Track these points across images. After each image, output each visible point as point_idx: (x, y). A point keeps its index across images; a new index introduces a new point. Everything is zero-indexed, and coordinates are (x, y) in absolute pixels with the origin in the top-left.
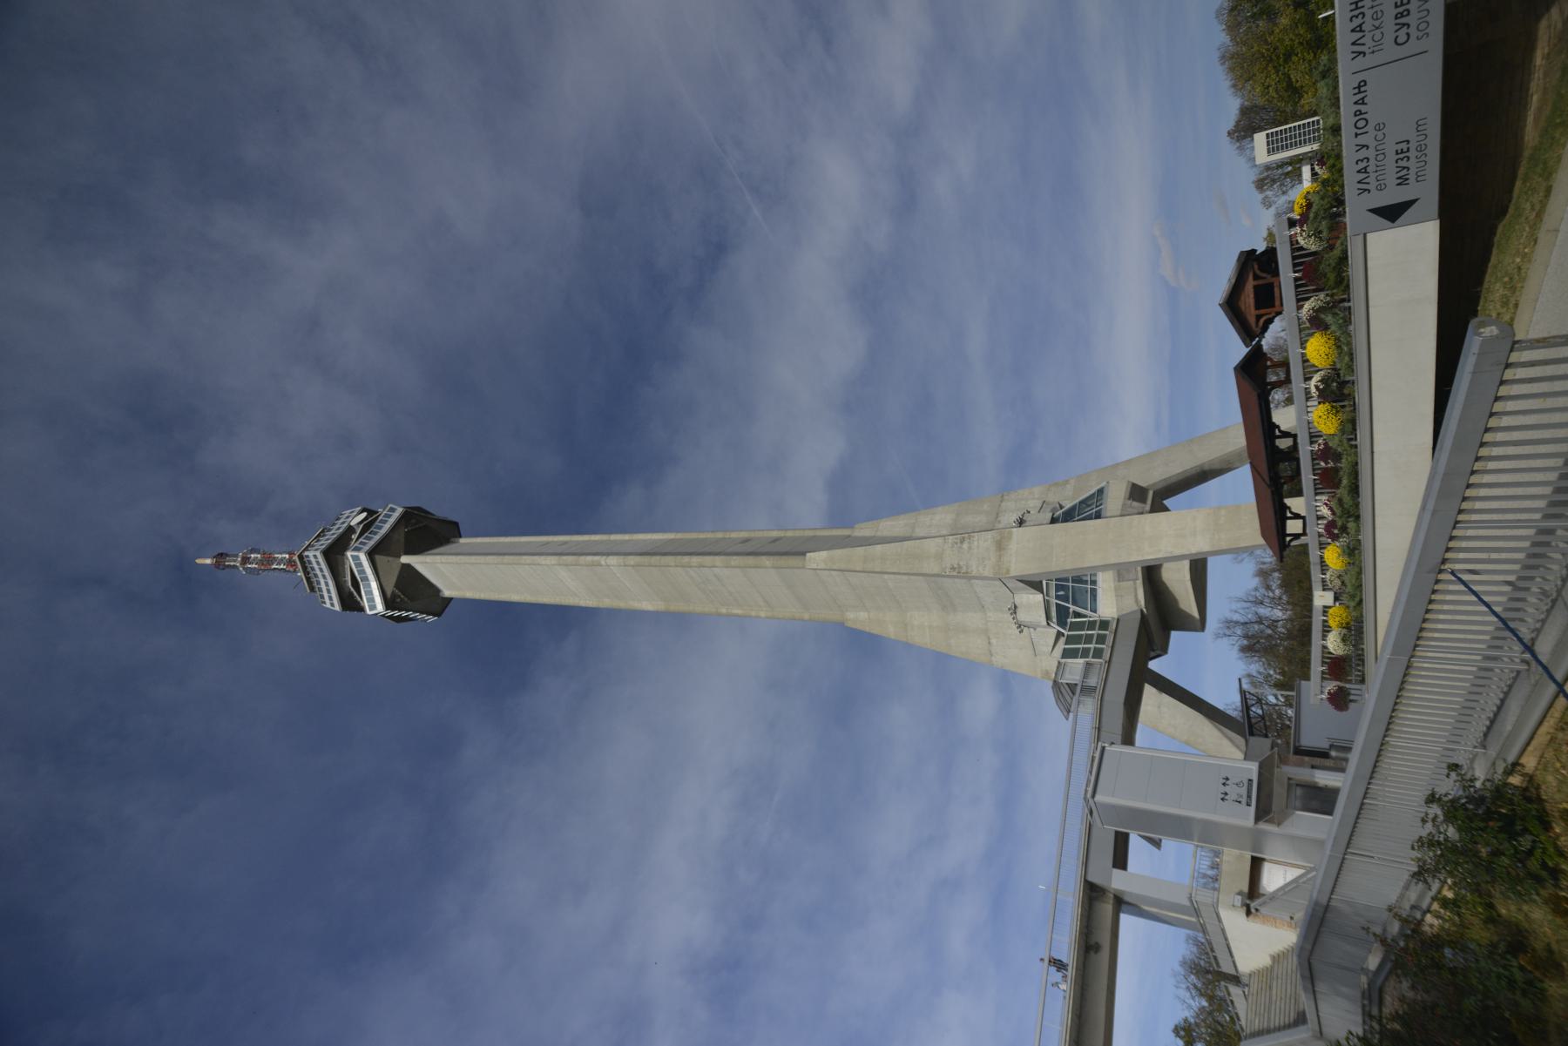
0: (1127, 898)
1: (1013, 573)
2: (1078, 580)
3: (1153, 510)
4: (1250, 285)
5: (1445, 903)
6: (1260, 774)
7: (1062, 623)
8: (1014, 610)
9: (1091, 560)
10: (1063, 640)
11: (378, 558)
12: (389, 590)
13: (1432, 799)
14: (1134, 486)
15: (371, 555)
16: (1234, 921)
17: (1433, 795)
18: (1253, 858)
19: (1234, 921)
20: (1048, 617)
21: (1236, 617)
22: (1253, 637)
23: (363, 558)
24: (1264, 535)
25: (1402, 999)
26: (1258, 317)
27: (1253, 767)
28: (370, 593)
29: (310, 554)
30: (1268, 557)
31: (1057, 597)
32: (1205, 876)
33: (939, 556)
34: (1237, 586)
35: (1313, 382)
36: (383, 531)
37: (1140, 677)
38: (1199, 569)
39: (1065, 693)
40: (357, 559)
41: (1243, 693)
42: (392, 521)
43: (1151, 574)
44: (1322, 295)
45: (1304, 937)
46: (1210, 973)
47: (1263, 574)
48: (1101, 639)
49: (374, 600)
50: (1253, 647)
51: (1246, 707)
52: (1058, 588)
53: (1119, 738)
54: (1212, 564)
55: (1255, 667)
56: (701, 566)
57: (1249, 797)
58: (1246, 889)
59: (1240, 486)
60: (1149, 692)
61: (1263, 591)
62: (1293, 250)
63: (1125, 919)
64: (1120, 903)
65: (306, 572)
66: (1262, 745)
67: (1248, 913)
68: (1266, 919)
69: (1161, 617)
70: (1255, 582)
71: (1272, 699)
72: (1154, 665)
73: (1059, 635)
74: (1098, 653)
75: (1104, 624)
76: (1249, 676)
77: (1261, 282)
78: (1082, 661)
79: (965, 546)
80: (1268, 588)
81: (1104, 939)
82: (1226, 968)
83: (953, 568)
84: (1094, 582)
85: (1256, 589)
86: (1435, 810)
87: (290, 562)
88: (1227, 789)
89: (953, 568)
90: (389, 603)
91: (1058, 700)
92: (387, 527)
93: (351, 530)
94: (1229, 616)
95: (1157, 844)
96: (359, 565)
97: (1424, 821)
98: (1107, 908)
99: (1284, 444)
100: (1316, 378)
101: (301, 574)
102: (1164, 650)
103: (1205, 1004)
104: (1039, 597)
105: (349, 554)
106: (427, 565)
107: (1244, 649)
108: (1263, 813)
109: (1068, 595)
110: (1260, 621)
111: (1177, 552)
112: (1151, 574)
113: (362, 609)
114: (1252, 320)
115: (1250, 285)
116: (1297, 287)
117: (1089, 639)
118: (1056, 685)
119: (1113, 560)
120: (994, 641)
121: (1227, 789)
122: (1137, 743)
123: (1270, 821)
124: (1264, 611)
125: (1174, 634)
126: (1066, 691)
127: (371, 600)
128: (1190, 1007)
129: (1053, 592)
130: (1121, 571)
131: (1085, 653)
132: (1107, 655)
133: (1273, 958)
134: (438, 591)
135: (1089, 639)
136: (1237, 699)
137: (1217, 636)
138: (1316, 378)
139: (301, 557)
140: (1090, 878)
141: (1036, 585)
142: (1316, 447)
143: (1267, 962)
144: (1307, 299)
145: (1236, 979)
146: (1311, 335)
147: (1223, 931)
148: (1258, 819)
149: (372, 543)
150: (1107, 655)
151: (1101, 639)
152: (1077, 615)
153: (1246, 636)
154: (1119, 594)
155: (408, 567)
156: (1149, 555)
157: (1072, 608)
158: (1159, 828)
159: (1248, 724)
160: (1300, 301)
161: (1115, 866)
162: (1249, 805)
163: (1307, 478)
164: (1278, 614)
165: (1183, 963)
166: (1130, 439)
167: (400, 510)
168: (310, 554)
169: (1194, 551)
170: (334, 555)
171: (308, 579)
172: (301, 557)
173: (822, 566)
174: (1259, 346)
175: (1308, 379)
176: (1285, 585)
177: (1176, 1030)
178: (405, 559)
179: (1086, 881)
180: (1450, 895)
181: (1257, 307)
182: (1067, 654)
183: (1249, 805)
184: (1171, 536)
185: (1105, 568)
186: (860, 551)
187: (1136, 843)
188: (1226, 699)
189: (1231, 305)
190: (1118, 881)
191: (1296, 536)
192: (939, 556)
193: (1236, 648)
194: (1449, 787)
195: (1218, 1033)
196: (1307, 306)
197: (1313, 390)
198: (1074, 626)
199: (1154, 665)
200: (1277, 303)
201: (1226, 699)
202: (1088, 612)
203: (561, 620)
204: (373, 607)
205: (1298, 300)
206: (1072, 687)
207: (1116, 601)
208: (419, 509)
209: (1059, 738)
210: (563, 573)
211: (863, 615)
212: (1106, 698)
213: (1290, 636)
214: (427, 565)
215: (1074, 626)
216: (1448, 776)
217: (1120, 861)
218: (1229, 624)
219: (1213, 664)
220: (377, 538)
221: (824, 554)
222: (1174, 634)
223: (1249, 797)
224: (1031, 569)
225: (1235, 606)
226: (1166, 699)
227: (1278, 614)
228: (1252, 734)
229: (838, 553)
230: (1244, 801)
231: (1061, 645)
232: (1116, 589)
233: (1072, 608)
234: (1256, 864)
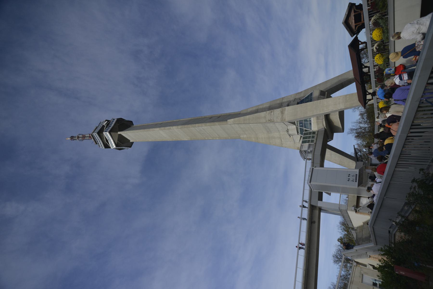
0: (322, 208)
1: (286, 120)
2: (306, 121)
3: (327, 97)
4: (353, 14)
5: (416, 211)
6: (359, 173)
7: (301, 134)
8: (288, 131)
9: (309, 114)
10: (302, 138)
11: (112, 133)
12: (116, 142)
13: (414, 181)
14: (321, 91)
15: (110, 132)
16: (352, 214)
17: (414, 179)
18: (357, 196)
19: (352, 214)
20: (298, 132)
21: (354, 128)
22: (358, 133)
23: (108, 133)
24: (359, 101)
25: (401, 237)
26: (356, 26)
27: (357, 171)
28: (111, 143)
29: (94, 134)
30: (362, 109)
31: (300, 126)
32: (346, 200)
33: (265, 117)
34: (354, 117)
35: (375, 47)
36: (112, 126)
37: (325, 147)
38: (341, 114)
39: (303, 153)
40: (107, 135)
41: (355, 149)
42: (114, 123)
43: (327, 117)
44: (378, 14)
45: (372, 219)
46: (346, 225)
47: (362, 115)
48: (313, 137)
49: (113, 145)
50: (359, 135)
51: (356, 153)
52: (300, 123)
53: (319, 165)
54: (346, 112)
55: (359, 142)
56: (199, 126)
57: (356, 179)
58: (355, 204)
59: (352, 88)
60: (328, 151)
61: (362, 119)
62: (372, 41)
63: (322, 214)
64: (320, 210)
65: (93, 138)
66: (361, 164)
67: (356, 212)
68: (361, 213)
69: (331, 129)
70: (360, 117)
71: (364, 150)
72: (329, 143)
73: (301, 136)
74: (312, 141)
75: (314, 133)
76: (358, 144)
77: (356, 13)
78: (308, 144)
79: (272, 113)
80: (363, 118)
81: (316, 220)
82: (350, 226)
83: (269, 120)
84: (310, 121)
85: (359, 119)
86: (415, 184)
87: (90, 137)
88: (349, 178)
89: (269, 120)
90: (117, 145)
91: (301, 155)
92: (113, 124)
93: (103, 126)
94: (352, 127)
95: (330, 194)
96: (107, 136)
97: (411, 189)
98: (317, 212)
99: (365, 70)
100: (376, 45)
101: (93, 140)
102: (332, 139)
103: (346, 233)
104: (295, 126)
105: (104, 133)
106: (126, 134)
107: (356, 137)
108: (360, 184)
109: (303, 126)
110: (361, 128)
111: (335, 109)
112: (327, 117)
113: (110, 148)
114: (354, 27)
115: (353, 14)
116: (369, 12)
117: (309, 137)
118: (301, 152)
119: (315, 114)
120: (283, 140)
121: (349, 178)
122: (325, 166)
123: (363, 186)
124: (362, 125)
125: (335, 134)
126: (304, 153)
127: (112, 145)
128: (342, 234)
129: (299, 125)
130: (318, 117)
131: (308, 142)
132: (315, 142)
133: (364, 223)
134: (129, 141)
135: (309, 137)
136: (353, 151)
137: (348, 133)
138: (376, 45)
139: (92, 135)
140: (312, 204)
141: (294, 123)
142: (375, 70)
143: (362, 224)
144: (373, 16)
145: (353, 229)
146: (374, 30)
147: (349, 216)
148: (359, 186)
149: (110, 129)
150: (315, 142)
151: (313, 137)
152: (306, 131)
153: (357, 133)
154: (318, 124)
155: (120, 134)
156: (326, 111)
157: (304, 129)
158: (330, 190)
159: (356, 158)
160: (370, 18)
161: (319, 200)
162: (356, 182)
163: (373, 80)
164: (366, 126)
165: (340, 223)
166: (317, 76)
167: (116, 119)
168: (94, 134)
169: (339, 109)
170: (100, 133)
171: (95, 141)
172: (92, 135)
173: (232, 123)
174: (356, 38)
175: (373, 46)
176: (368, 117)
177: (338, 240)
178: (119, 133)
179: (311, 205)
180: (417, 209)
181: (355, 23)
182: (303, 142)
183: (356, 182)
184: (330, 105)
185: (313, 116)
186: (242, 118)
187: (325, 195)
188: (351, 151)
189: (346, 23)
190: (320, 204)
191: (370, 100)
192: (265, 117)
193: (354, 136)
194: (419, 176)
195: (350, 240)
196: (373, 19)
197: (375, 49)
198: (305, 134)
199: (329, 143)
200: (362, 20)
201: (351, 151)
202: (309, 130)
203: (176, 145)
204: (113, 147)
205: (369, 17)
206: (305, 151)
207: (317, 126)
208: (121, 119)
209: (301, 167)
210: (161, 132)
211: (245, 136)
212: (315, 153)
213: (369, 132)
214: (126, 134)
215: (305, 134)
216: (420, 173)
217: (320, 198)
218: (352, 130)
219: (346, 141)
220: (111, 128)
221: (232, 120)
222: (335, 134)
223: (356, 179)
224: (292, 119)
225: (353, 124)
226: (333, 153)
227: (366, 126)
228: (358, 161)
229: (236, 119)
230: (355, 181)
231: (302, 140)
232: (317, 122)
233: (304, 129)
234: (358, 198)
